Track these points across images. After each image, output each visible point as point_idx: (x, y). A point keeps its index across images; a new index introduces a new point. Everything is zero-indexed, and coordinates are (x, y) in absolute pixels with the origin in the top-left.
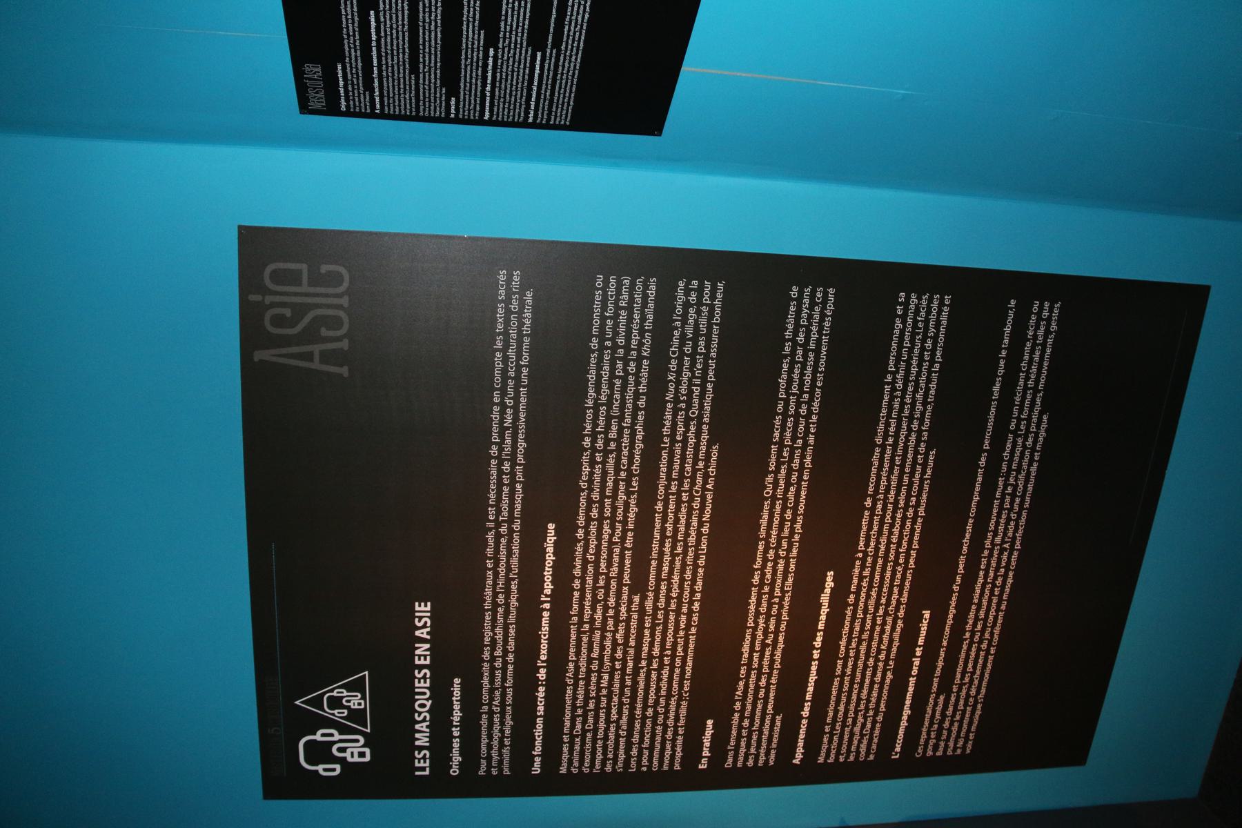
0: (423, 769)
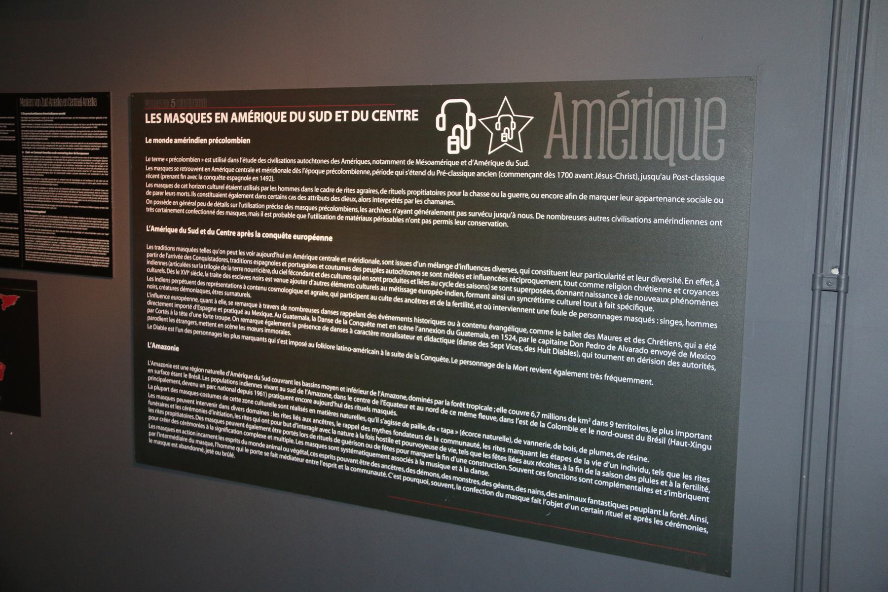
0: (149, 119)
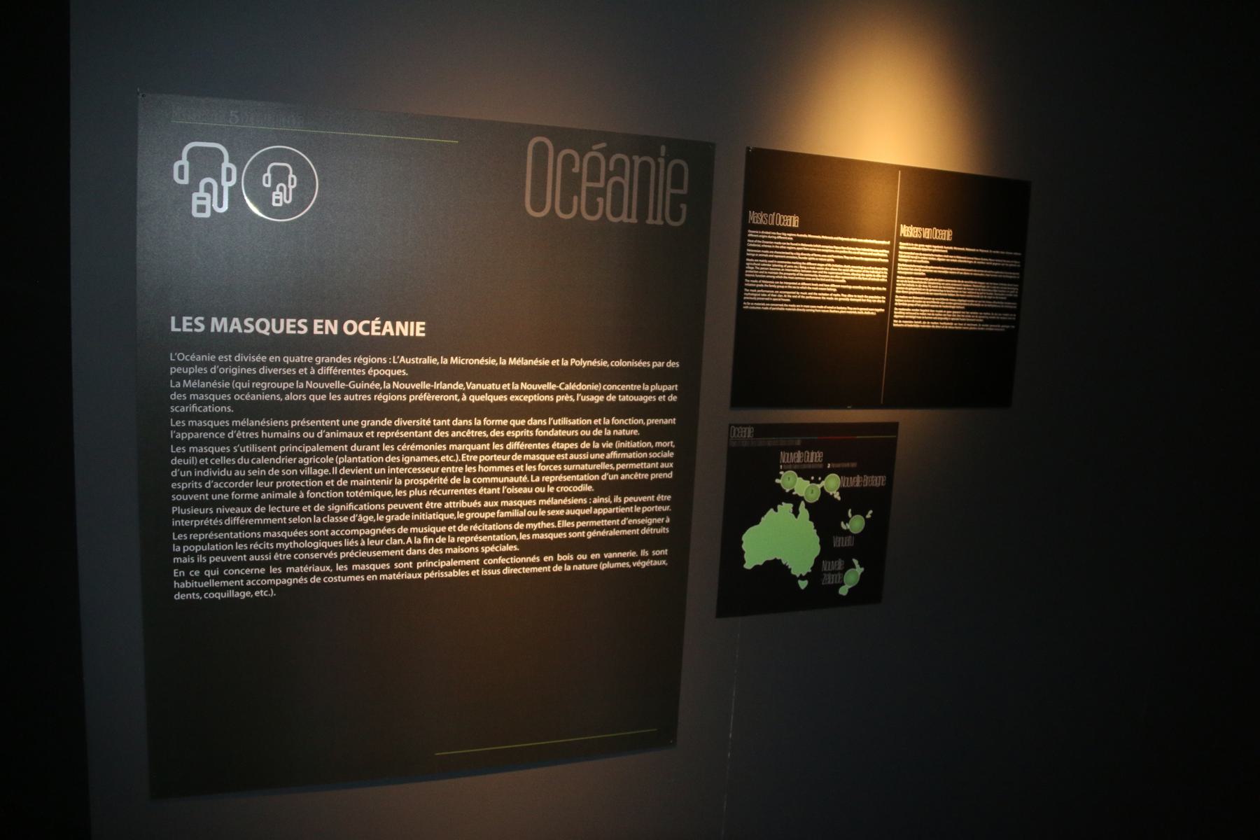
0: (179, 324)
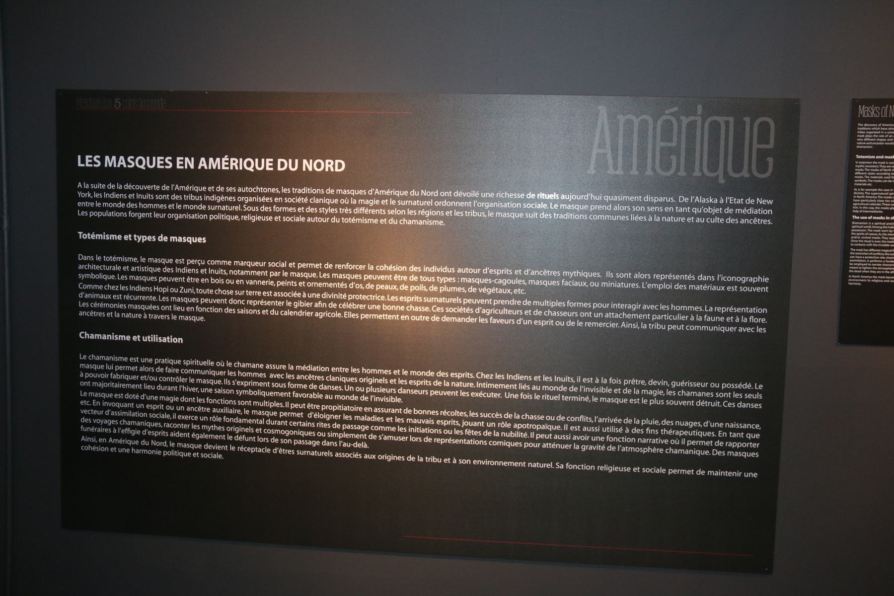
0: (83, 161)
